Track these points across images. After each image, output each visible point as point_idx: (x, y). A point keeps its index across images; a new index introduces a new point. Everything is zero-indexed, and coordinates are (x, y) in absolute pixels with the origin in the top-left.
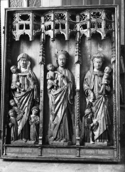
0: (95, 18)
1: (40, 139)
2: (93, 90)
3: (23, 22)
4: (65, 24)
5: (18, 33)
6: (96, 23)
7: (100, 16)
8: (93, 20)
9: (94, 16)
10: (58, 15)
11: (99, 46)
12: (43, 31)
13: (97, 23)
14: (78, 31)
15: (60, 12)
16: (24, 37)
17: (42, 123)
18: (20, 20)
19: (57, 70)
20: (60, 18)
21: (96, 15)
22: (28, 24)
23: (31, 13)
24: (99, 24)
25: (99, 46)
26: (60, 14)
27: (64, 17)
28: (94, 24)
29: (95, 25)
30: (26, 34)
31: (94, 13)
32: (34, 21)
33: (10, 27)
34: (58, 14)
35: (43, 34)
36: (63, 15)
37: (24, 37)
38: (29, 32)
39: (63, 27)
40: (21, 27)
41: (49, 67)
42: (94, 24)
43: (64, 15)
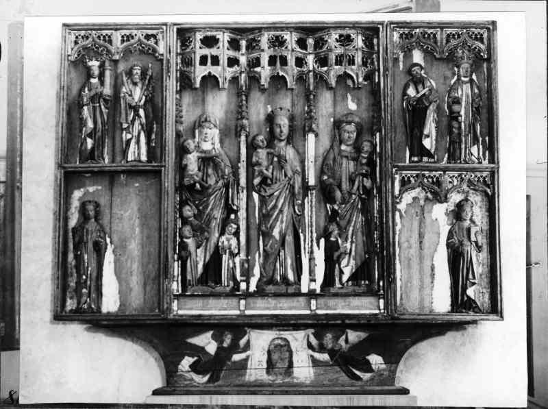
5: (200, 72)
7: (352, 41)
9: (340, 41)
14: (311, 71)
15: (278, 33)
21: (344, 40)
31: (341, 36)
39: (351, 62)
40: (339, 61)
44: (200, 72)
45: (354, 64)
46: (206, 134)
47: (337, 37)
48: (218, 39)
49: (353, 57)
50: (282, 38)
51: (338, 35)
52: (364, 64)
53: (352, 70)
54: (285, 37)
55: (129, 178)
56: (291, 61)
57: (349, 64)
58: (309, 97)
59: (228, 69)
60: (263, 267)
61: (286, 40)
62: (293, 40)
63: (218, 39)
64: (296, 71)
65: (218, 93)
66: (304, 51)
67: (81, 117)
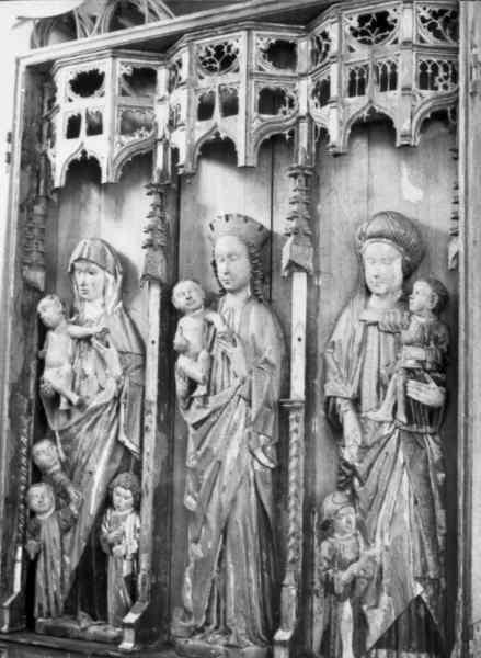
0: (370, 43)
1: (283, 644)
2: (356, 402)
3: (82, 105)
4: (235, 91)
5: (62, 152)
6: (370, 66)
7: (392, 28)
8: (361, 54)
9: (364, 33)
10: (209, 54)
11: (405, 179)
12: (160, 136)
13: (376, 69)
14: (303, 118)
15: (218, 40)
16: (85, 169)
17: (146, 552)
18: (127, 89)
19: (215, 310)
20: (218, 65)
21: (372, 28)
22: (260, 94)
23: (109, 61)
24: (385, 68)
25: (405, 179)
26: (219, 49)
27: (234, 57)
28: (362, 73)
29: (365, 76)
30: (88, 156)
31: (363, 19)
32: (124, 93)
33: (35, 132)
34: (211, 47)
35: (160, 148)
36: (229, 49)
37: (85, 169)
38: (105, 149)
39: (230, 108)
40: (356, 86)
41: (183, 293)
42: (362, 73)
43: (233, 49)
44: (62, 152)
45: (393, 87)
46: (83, 285)
47: (355, 23)
48: (103, 74)
49: (394, 67)
50: (229, 49)
51: (355, 18)
52: (425, 80)
53: (390, 103)
54: (236, 46)
55: (284, 625)
56: (247, 97)
57: (384, 89)
58: (174, 188)
59: (198, 123)
60: (236, 571)
61: (237, 52)
62: (255, 50)
63: (103, 74)
64: (256, 124)
65: (196, 186)
66: (289, 73)
67: (41, 355)
